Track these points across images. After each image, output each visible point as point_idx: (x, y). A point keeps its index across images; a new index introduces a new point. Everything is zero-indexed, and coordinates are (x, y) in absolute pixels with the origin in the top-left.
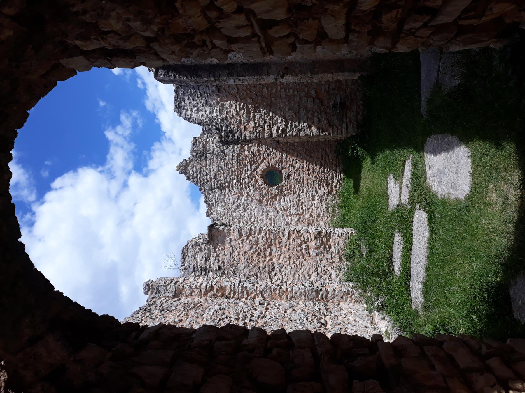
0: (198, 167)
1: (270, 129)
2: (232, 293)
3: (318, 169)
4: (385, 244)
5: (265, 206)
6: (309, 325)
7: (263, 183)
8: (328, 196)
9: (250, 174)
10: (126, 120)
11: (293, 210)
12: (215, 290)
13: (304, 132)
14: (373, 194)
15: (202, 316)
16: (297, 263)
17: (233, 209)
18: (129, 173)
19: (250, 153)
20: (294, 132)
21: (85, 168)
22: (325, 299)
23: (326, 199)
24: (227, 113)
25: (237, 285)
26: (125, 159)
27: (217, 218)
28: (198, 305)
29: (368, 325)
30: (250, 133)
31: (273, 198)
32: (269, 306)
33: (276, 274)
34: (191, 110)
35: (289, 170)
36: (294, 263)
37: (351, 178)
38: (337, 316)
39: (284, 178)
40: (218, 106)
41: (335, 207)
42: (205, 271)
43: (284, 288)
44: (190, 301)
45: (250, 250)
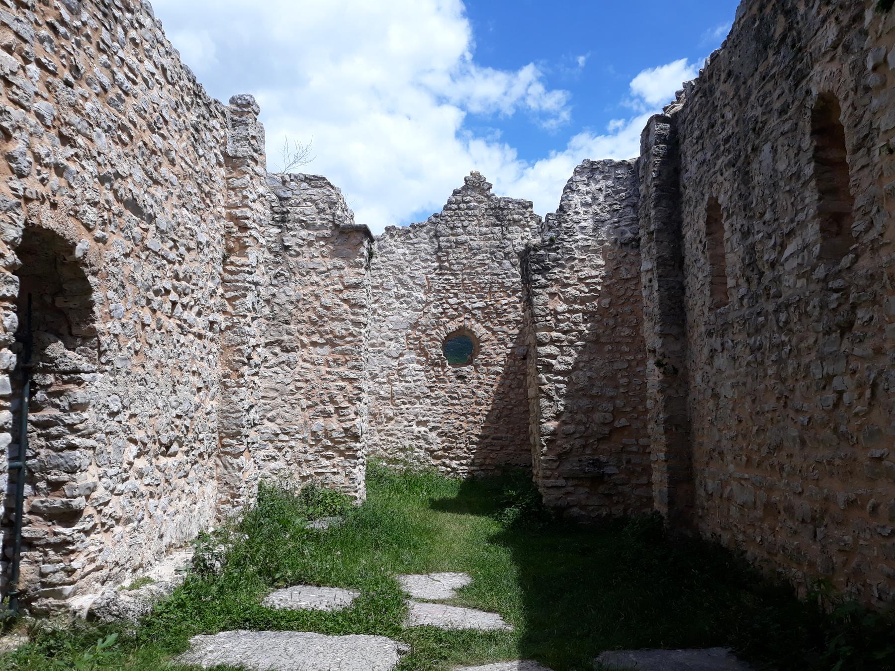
0: (476, 212)
1: (552, 342)
2: (234, 268)
3: (476, 431)
4: (332, 569)
5: (407, 335)
6: (165, 421)
7: (448, 331)
8: (427, 449)
9: (465, 308)
10: (554, 100)
11: (399, 386)
12: (240, 234)
13: (546, 407)
14: (429, 538)
15: (183, 206)
16: (298, 396)
17: (400, 276)
18: (462, 107)
19: (505, 307)
20: (547, 387)
21: (469, 32)
22: (223, 451)
23: (420, 447)
24: (582, 260)
25: (249, 278)
26: (486, 99)
27: (384, 247)
28: (208, 201)
29: (166, 540)
30: (545, 304)
31: (421, 349)
32: (206, 342)
33: (276, 354)
34: (588, 193)
35: (473, 378)
36: (298, 389)
37: (460, 493)
38: (185, 476)
39: (458, 369)
40: (594, 244)
41: (406, 463)
42: (282, 220)
43: (245, 370)
44: (216, 186)
45: (322, 306)
